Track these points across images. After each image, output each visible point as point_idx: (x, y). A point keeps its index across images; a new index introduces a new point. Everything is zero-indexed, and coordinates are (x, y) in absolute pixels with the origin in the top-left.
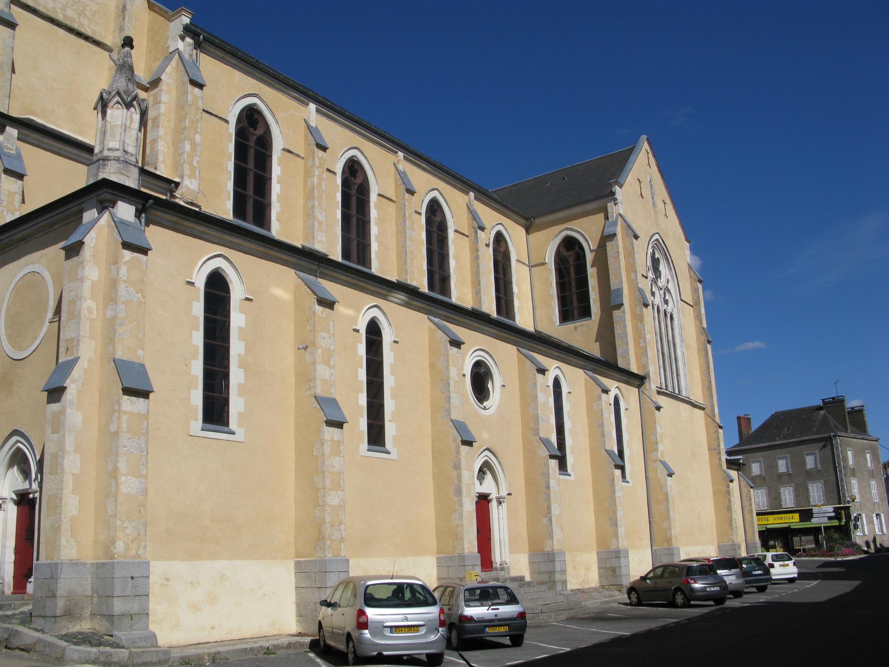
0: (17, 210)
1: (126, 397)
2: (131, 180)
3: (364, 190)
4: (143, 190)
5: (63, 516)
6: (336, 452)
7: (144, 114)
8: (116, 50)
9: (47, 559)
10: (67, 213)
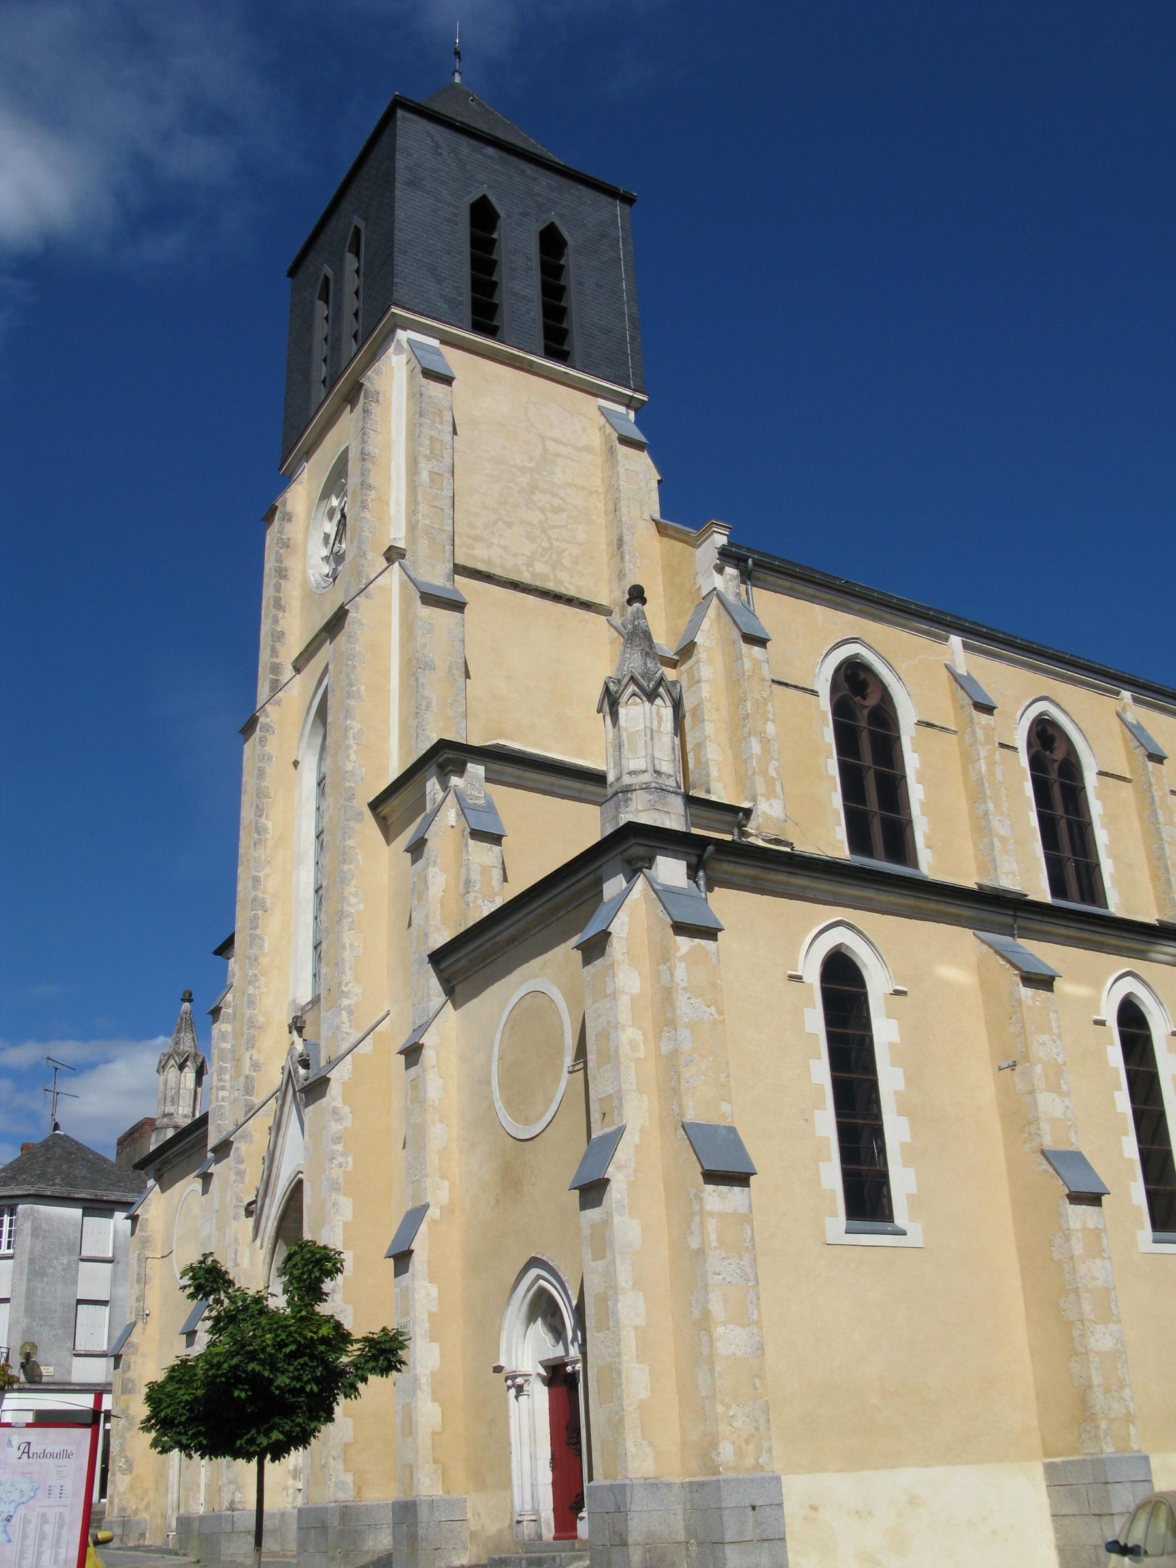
0: (497, 894)
1: (710, 1188)
2: (673, 818)
3: (1071, 769)
4: (695, 831)
5: (626, 1402)
6: (1096, 1249)
7: (677, 706)
8: (617, 610)
9: (605, 1478)
10: (578, 886)
